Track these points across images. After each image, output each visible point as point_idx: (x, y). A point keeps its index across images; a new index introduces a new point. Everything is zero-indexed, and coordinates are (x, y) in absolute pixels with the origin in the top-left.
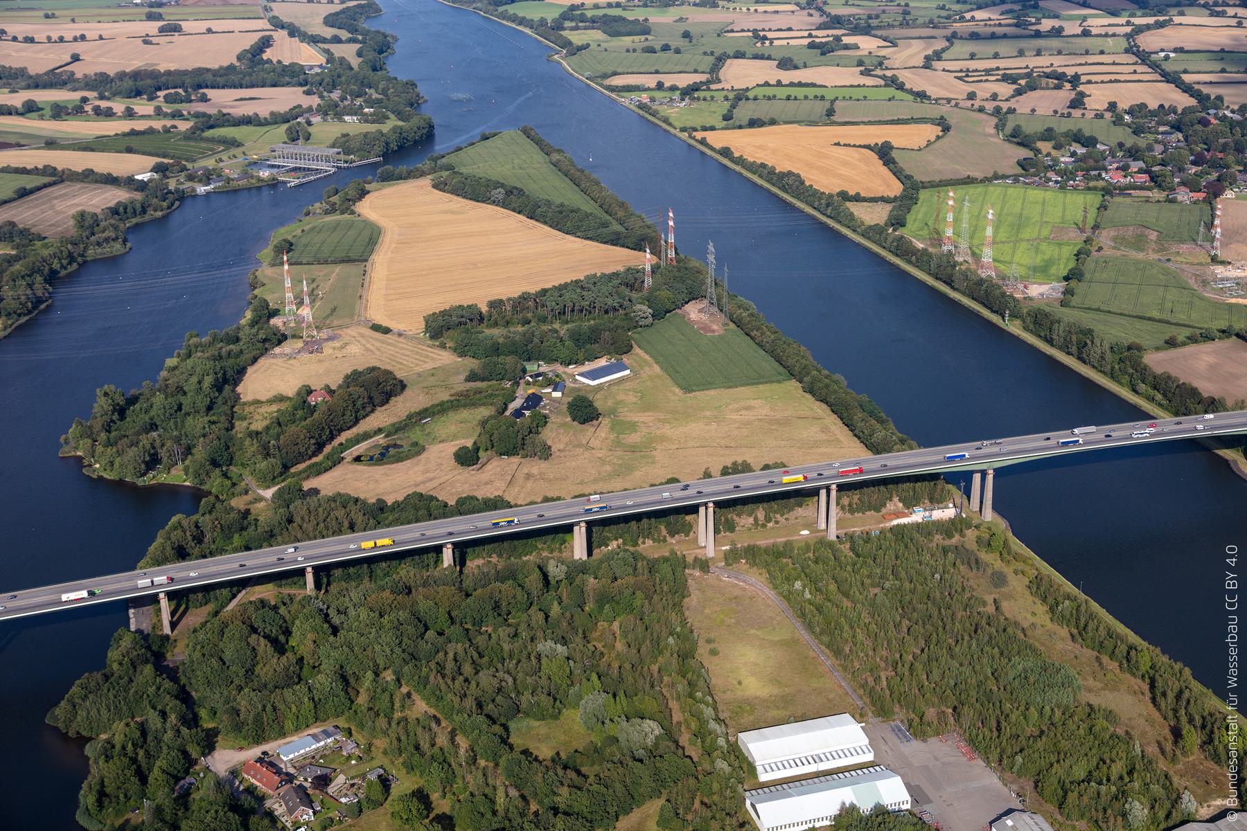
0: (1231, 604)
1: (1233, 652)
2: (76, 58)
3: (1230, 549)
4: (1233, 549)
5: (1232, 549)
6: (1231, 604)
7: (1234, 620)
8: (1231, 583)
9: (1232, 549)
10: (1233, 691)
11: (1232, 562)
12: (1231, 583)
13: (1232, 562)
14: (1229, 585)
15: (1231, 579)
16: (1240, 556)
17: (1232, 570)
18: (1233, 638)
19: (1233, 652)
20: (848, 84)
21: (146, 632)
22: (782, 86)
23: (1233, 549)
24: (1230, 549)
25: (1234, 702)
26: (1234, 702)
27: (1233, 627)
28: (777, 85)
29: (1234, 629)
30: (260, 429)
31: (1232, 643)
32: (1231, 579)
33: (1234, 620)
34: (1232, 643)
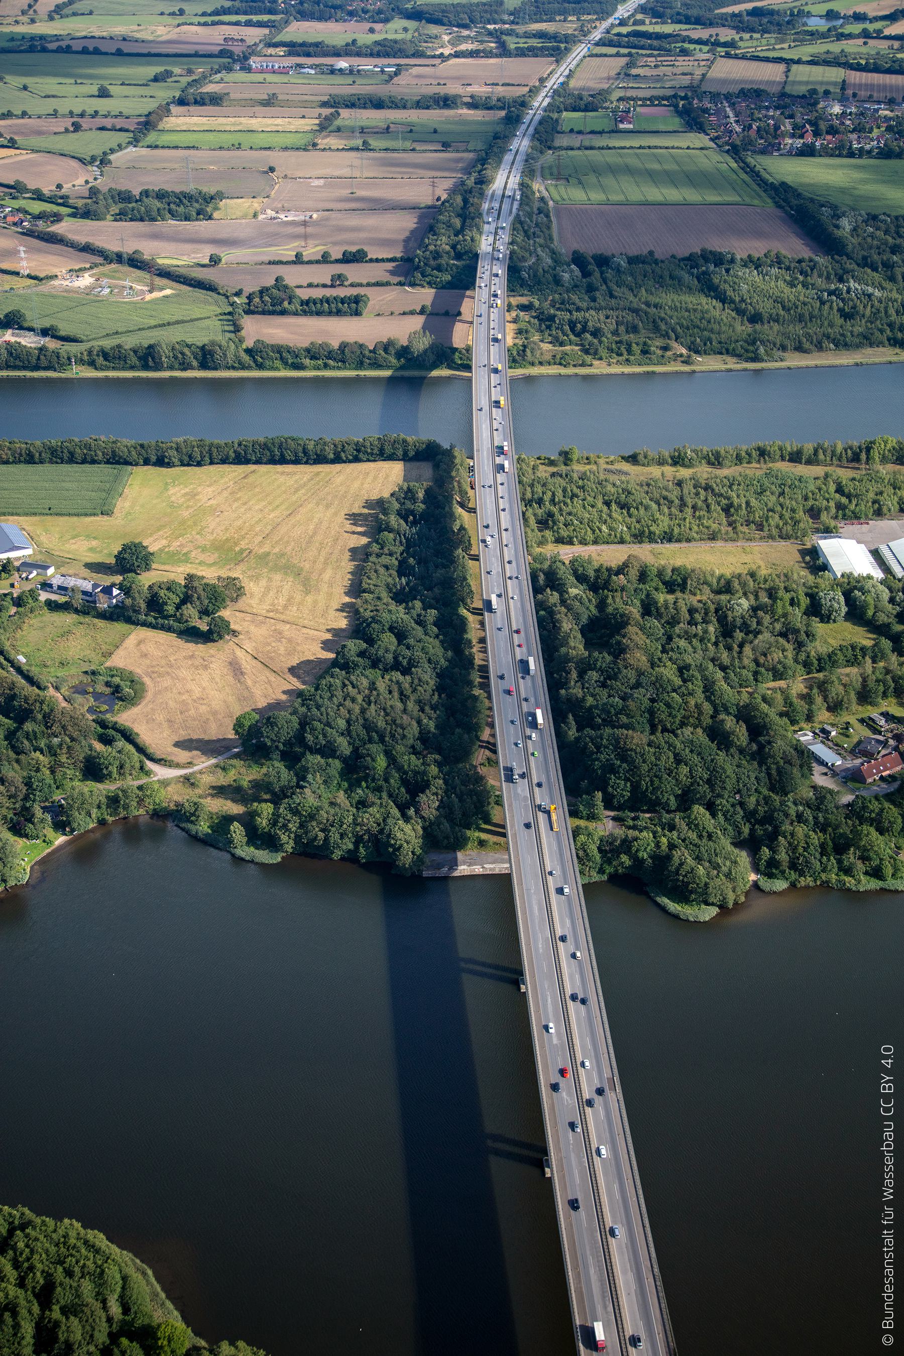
0: (887, 1109)
1: (889, 1161)
2: (215, 261)
3: (886, 1050)
4: (889, 1050)
5: (888, 1341)
6: (887, 1109)
7: (890, 1126)
8: (887, 1086)
9: (887, 1049)
10: (889, 1203)
11: (888, 1063)
12: (887, 1086)
13: (888, 1063)
14: (884, 1088)
15: (886, 1082)
16: (896, 1057)
17: (888, 1072)
18: (888, 1146)
19: (889, 1161)
20: (365, 282)
21: (342, 623)
22: (302, 263)
23: (889, 1050)
24: (886, 1050)
25: (890, 1215)
26: (890, 1215)
27: (888, 1195)
28: (294, 263)
29: (890, 1136)
30: (838, 567)
31: (888, 1152)
32: (886, 1082)
33: (890, 1126)
34: (888, 1152)
